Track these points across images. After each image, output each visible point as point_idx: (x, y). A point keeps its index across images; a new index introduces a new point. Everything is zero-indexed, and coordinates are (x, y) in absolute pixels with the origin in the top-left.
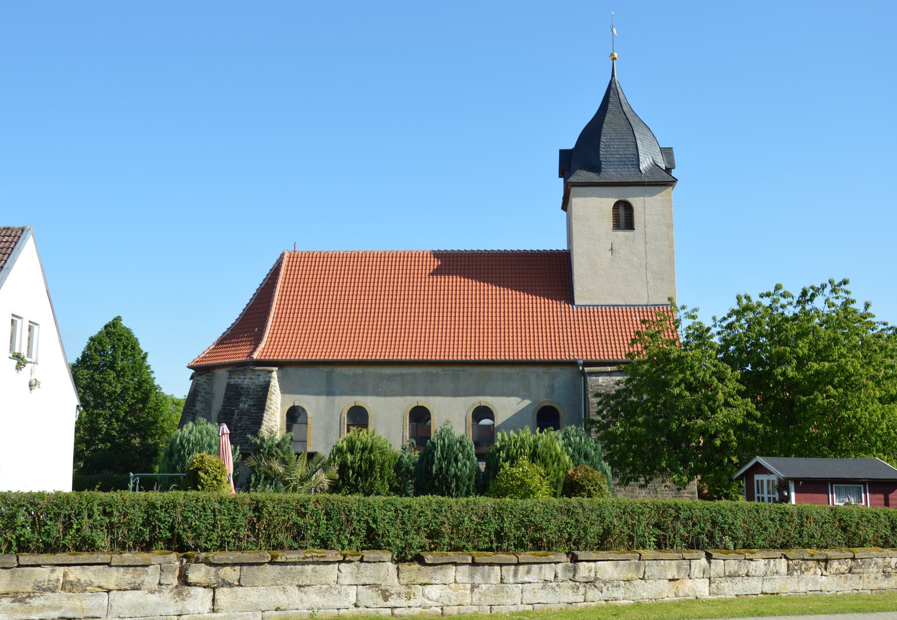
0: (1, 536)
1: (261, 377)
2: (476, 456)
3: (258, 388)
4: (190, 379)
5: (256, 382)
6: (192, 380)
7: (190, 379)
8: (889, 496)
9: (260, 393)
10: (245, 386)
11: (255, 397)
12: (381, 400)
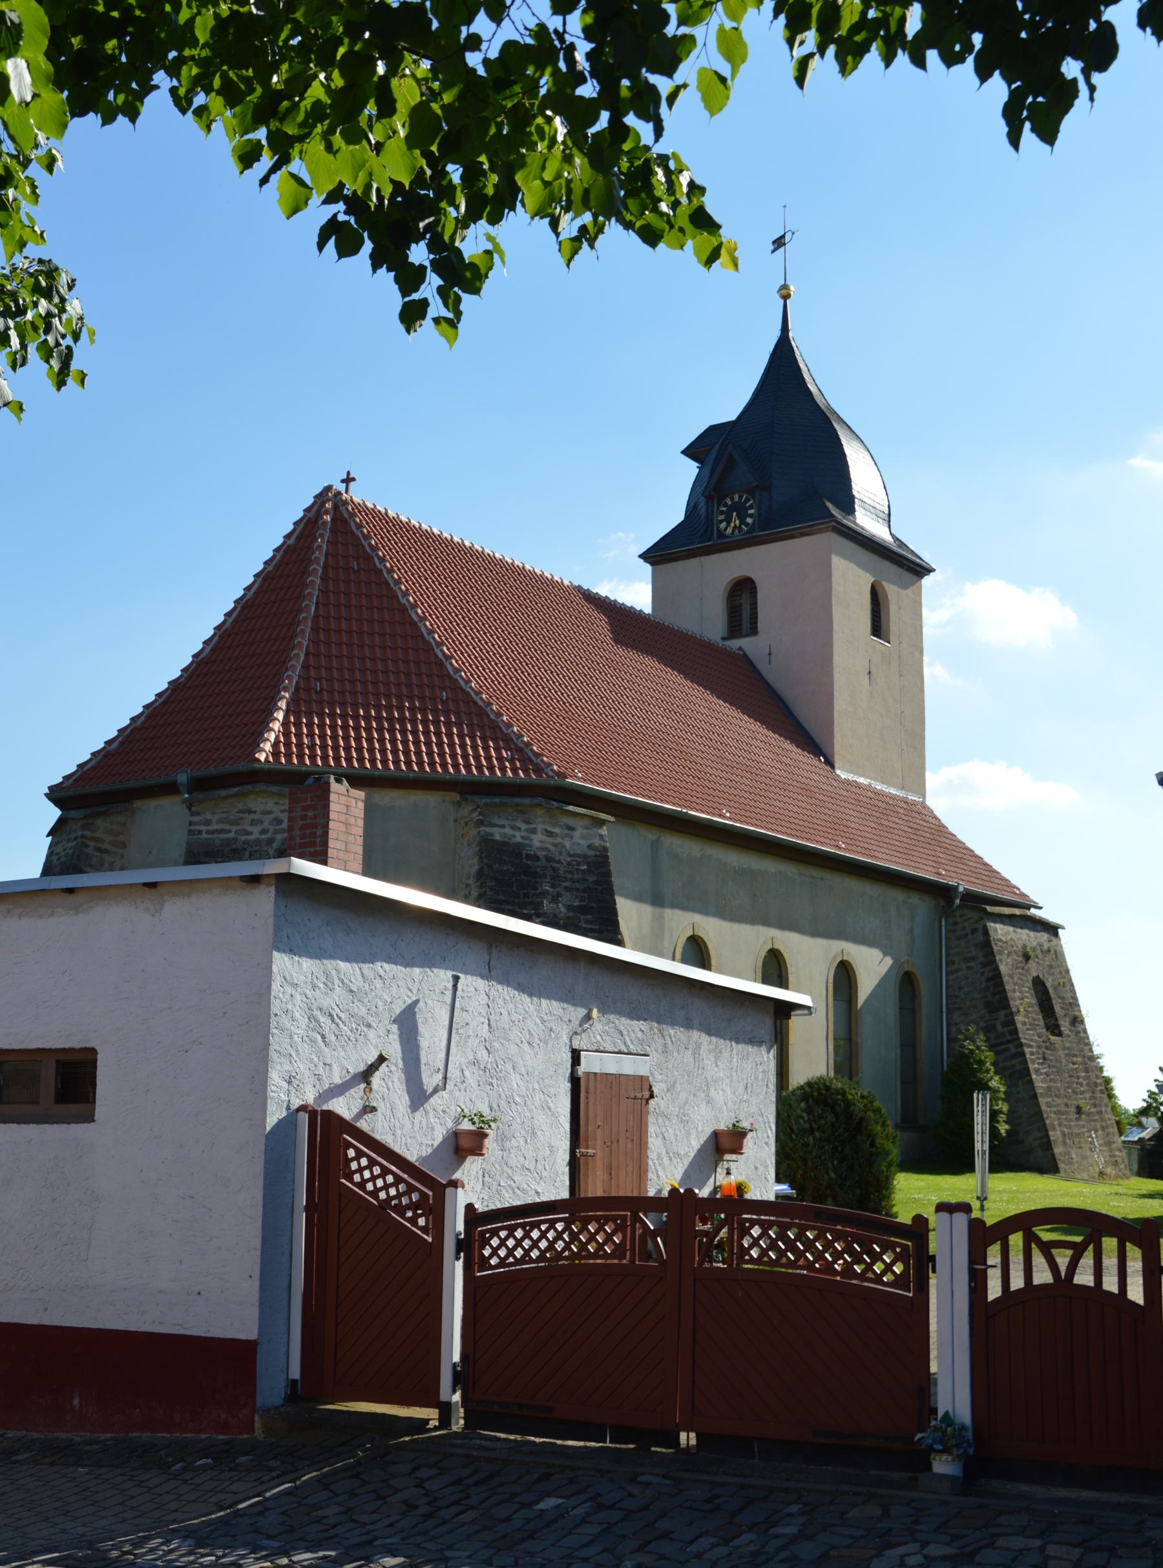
0: (2, 300)
1: (577, 834)
2: (1140, 1139)
3: (579, 863)
4: (48, 836)
5: (567, 844)
6: (50, 838)
7: (48, 836)
8: (480, 1210)
9: (592, 878)
10: (541, 854)
11: (577, 885)
12: (727, 927)
